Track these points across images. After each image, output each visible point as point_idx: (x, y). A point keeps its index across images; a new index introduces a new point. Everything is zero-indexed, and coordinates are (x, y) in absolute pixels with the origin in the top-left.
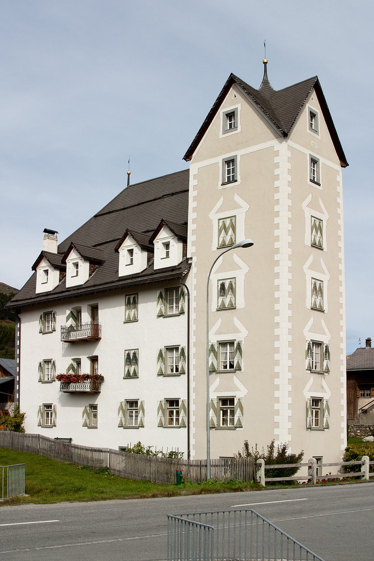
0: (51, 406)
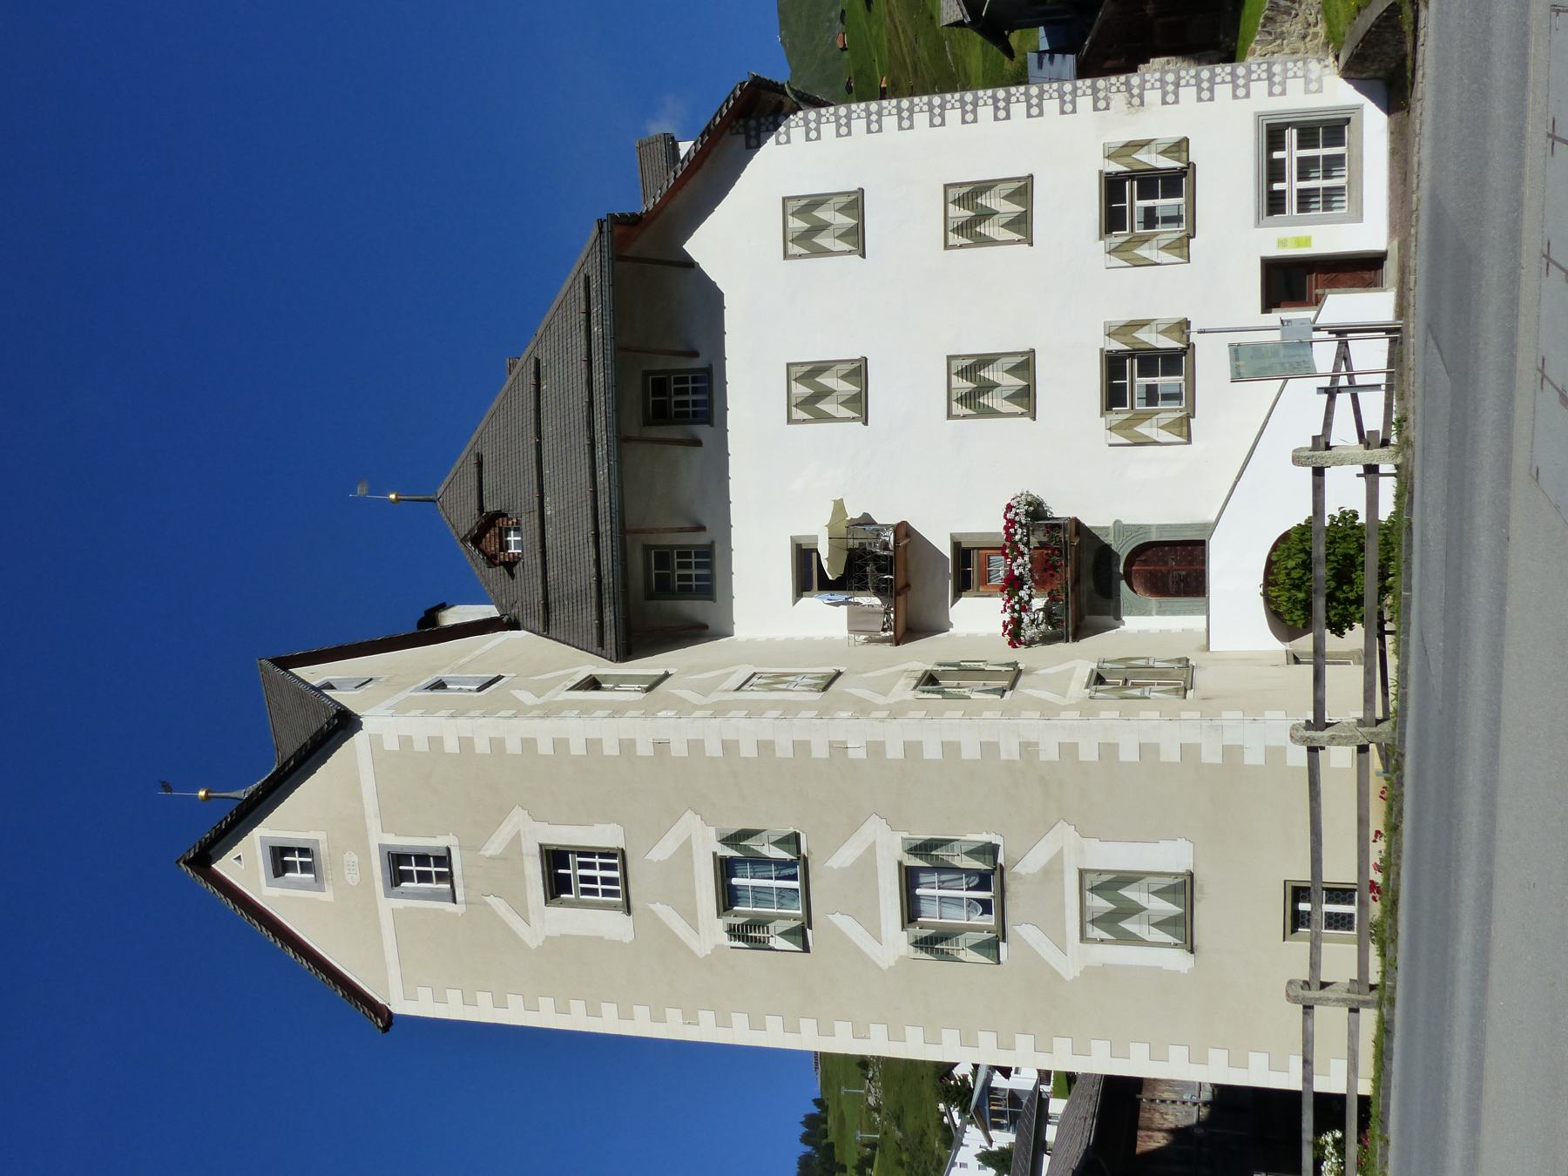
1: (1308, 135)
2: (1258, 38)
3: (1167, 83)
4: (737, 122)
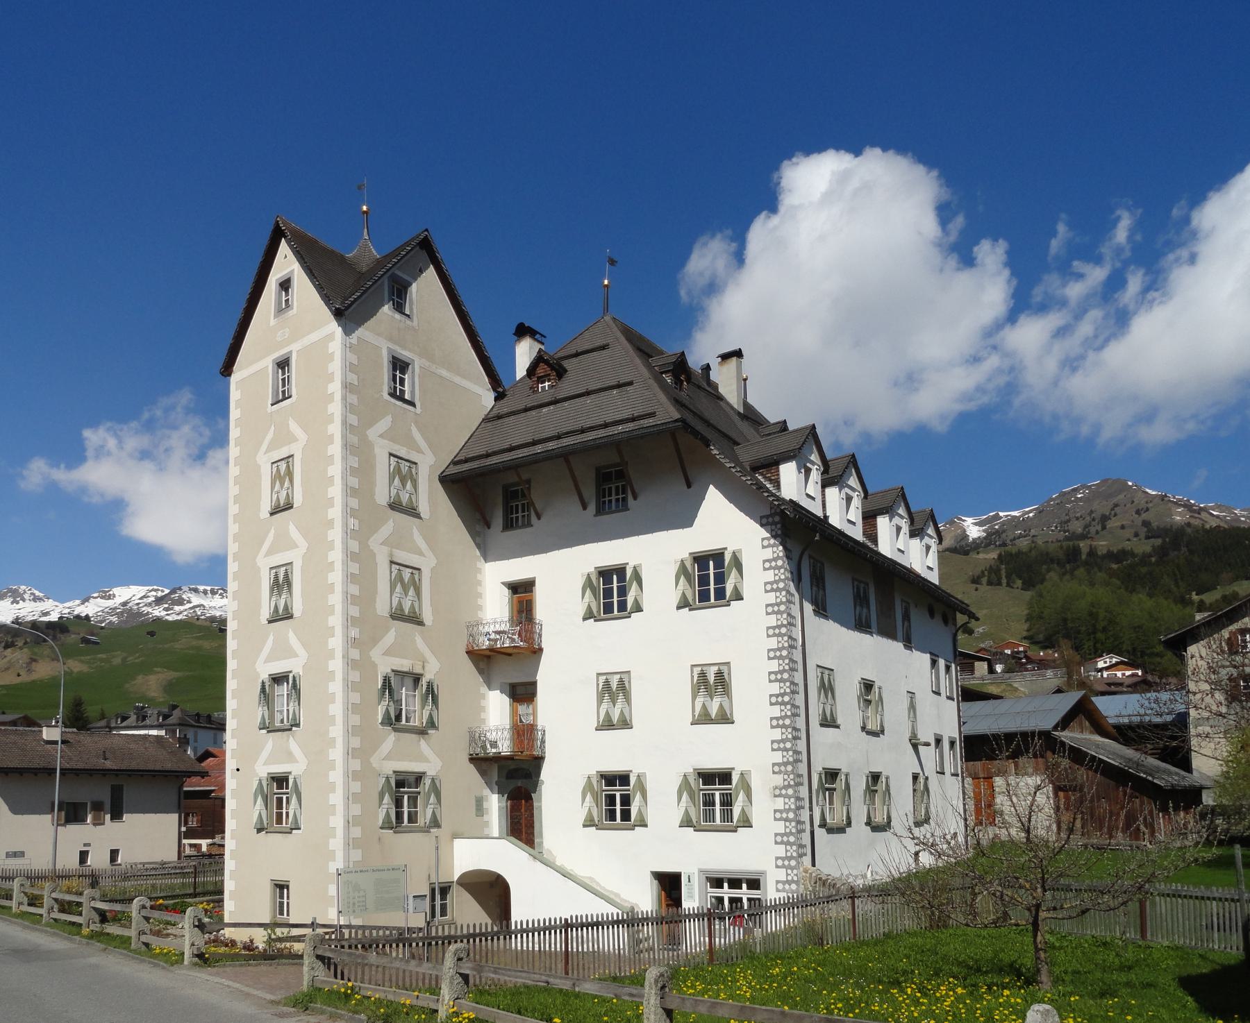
0: (286, 779)
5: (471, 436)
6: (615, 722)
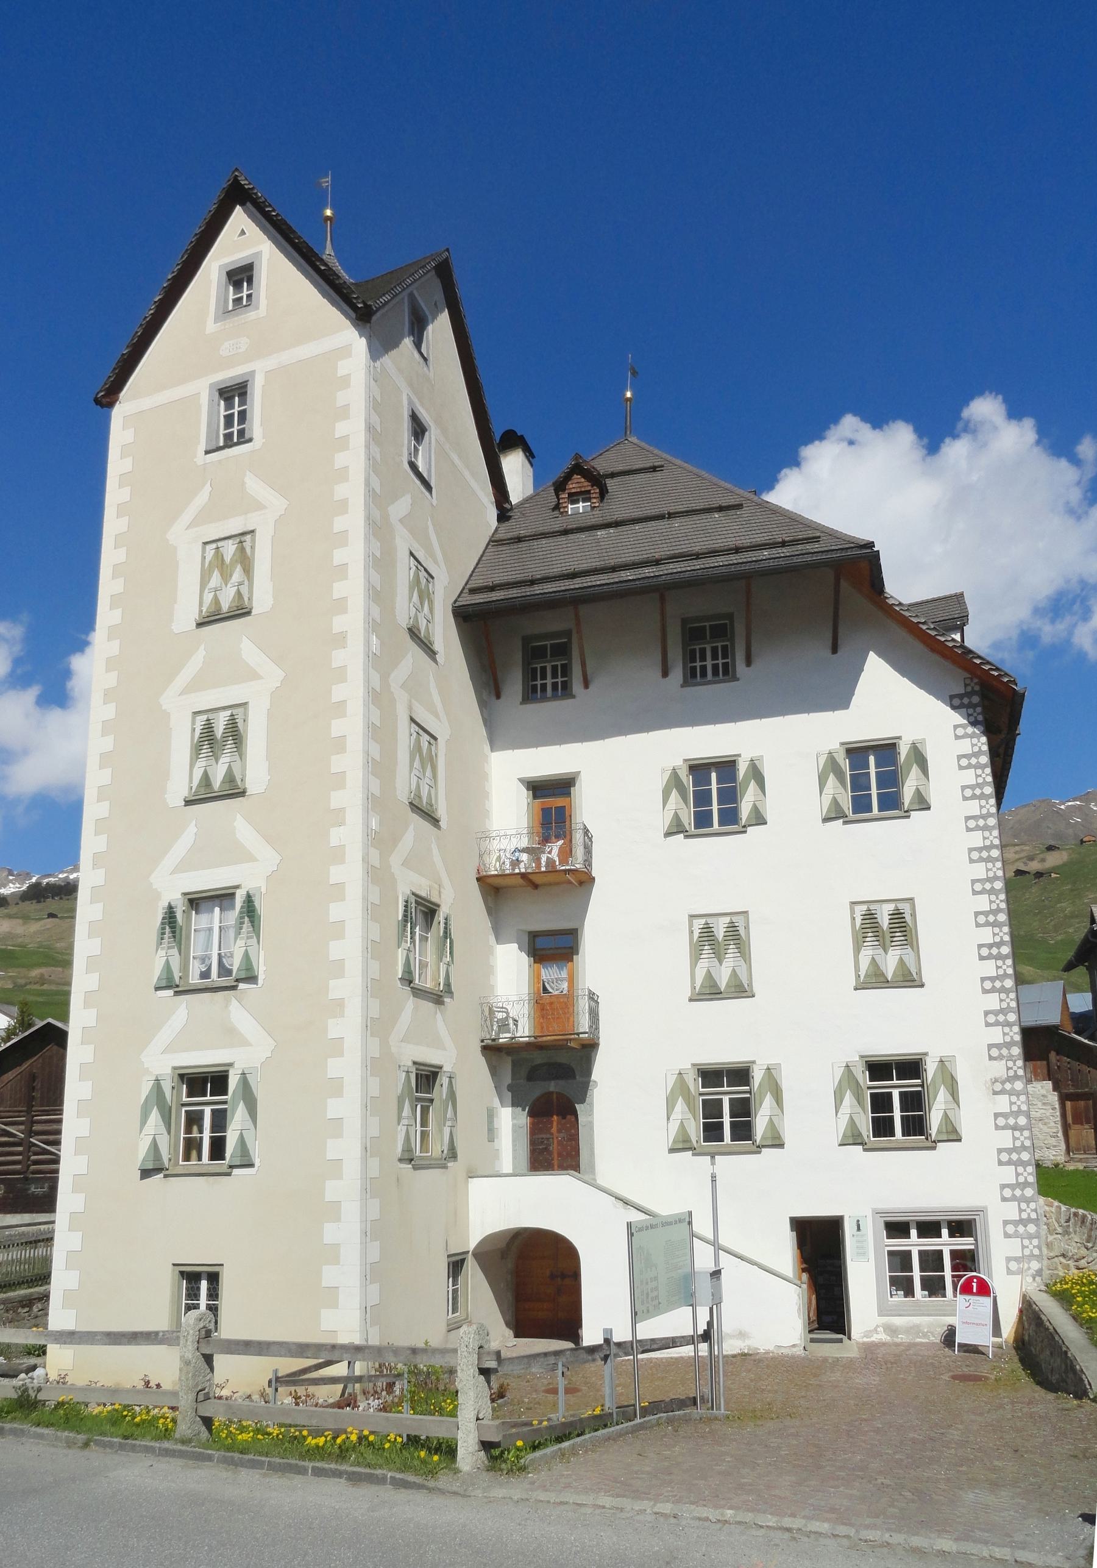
1: (965, 1261)
2: (1063, 1208)
3: (1016, 1118)
4: (976, 684)
5: (480, 560)
6: (723, 986)
